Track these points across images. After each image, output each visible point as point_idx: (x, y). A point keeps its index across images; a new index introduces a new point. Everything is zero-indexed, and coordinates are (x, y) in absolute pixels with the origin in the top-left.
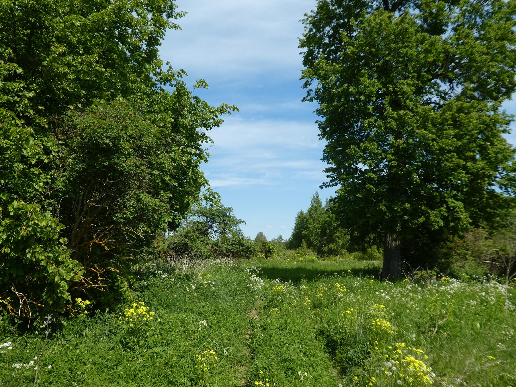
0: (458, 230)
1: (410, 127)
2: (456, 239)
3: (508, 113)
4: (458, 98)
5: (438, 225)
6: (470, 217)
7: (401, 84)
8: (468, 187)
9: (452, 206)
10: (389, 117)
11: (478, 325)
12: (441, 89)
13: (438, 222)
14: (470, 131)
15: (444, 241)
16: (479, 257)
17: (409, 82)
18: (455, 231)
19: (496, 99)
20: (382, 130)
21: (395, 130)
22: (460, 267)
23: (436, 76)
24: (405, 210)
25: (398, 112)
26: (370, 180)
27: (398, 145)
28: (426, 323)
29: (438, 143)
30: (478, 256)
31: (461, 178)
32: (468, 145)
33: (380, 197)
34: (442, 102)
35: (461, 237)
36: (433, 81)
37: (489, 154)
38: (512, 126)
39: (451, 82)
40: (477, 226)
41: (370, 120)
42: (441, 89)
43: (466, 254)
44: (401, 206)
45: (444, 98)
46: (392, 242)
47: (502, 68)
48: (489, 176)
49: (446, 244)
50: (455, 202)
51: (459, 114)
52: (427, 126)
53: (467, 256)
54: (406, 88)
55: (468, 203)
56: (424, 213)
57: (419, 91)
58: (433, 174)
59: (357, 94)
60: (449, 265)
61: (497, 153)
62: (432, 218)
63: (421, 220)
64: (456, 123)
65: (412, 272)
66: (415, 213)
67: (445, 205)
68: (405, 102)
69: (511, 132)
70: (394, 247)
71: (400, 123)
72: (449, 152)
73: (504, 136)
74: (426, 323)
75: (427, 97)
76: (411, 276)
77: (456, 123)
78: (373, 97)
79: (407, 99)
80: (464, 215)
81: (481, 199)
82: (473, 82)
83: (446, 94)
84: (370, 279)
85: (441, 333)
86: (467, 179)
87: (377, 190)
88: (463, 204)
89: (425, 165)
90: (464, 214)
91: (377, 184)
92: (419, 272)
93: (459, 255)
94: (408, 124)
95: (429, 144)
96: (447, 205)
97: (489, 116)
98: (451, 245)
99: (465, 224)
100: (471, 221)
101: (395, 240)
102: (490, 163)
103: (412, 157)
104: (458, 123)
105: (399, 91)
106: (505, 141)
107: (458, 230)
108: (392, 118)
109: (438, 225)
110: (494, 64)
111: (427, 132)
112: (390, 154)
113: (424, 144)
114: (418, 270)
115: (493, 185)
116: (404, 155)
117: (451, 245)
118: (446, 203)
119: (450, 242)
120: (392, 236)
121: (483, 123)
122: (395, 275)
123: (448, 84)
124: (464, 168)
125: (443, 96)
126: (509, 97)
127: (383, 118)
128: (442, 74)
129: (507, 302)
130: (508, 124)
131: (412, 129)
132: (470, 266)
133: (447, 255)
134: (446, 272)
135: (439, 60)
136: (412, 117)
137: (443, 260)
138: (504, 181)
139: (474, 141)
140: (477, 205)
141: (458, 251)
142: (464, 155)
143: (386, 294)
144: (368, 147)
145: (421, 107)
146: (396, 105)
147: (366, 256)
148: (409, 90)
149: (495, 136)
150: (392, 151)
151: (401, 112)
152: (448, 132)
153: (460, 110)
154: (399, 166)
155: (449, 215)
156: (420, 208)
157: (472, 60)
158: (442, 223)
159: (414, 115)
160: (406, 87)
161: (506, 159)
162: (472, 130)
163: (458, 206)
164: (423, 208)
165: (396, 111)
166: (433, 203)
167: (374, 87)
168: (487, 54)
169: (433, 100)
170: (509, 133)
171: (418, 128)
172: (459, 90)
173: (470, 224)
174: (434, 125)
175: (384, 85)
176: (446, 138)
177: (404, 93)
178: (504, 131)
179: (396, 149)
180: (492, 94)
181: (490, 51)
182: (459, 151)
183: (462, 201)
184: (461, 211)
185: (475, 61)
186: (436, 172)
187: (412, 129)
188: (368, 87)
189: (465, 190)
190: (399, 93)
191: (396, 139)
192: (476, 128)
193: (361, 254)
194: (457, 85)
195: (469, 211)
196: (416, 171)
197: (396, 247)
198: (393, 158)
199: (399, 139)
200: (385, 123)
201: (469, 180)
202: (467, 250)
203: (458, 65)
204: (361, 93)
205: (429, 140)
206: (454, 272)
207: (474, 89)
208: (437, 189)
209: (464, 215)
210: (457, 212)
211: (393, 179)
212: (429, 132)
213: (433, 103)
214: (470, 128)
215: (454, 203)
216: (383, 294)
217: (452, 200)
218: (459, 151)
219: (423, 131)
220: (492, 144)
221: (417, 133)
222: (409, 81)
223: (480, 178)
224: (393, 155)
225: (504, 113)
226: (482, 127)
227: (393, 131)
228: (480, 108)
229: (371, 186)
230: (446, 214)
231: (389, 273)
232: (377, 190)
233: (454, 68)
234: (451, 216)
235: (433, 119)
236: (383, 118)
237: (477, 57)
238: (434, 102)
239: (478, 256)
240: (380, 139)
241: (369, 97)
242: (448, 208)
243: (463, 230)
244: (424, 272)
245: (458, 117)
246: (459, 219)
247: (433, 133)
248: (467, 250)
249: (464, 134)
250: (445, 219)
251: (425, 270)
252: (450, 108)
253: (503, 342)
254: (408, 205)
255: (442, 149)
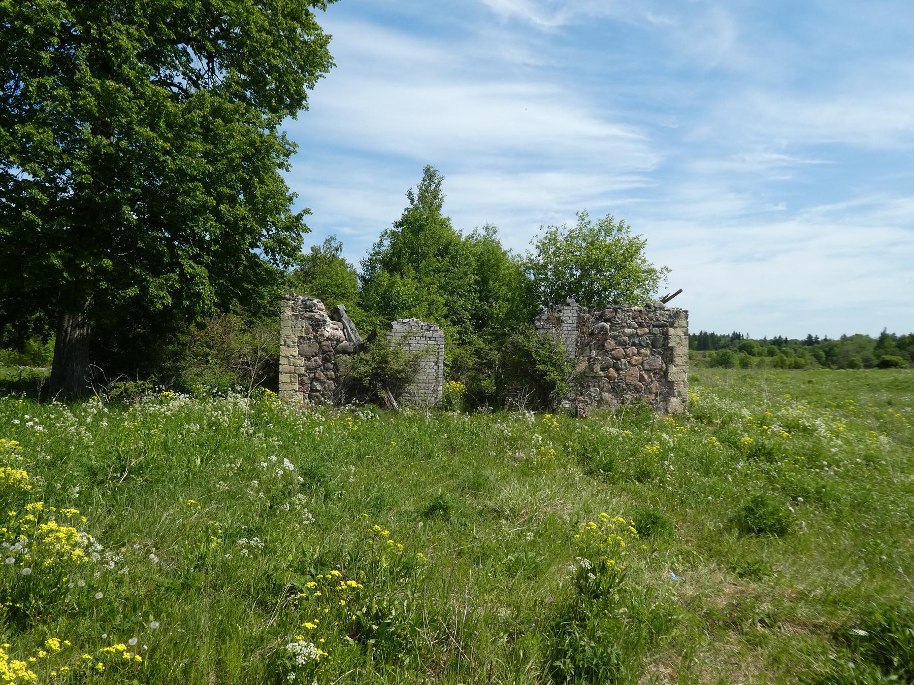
0: (195, 314)
1: (126, 116)
2: (193, 328)
3: (290, 138)
4: (214, 92)
5: (163, 304)
6: (217, 294)
7: (114, 29)
8: (219, 244)
9: (190, 274)
10: (83, 87)
11: (198, 461)
12: (192, 65)
13: (163, 298)
14: (230, 152)
15: (173, 331)
16: (227, 358)
17: (131, 31)
18: (190, 314)
19: (274, 110)
20: (66, 108)
21: (94, 115)
22: (196, 375)
23: (188, 41)
24: (101, 271)
25: (104, 82)
26: (32, 203)
27: (98, 146)
28: (109, 466)
29: (174, 160)
30: (226, 359)
31: (208, 230)
32: (224, 175)
33: (53, 242)
34: (193, 90)
35: (201, 326)
36: (180, 46)
37: (255, 196)
38: (292, 160)
39: (210, 59)
40: (227, 310)
41: (42, 80)
42: (192, 65)
43: (208, 355)
44: (94, 262)
45: (196, 85)
46: (74, 328)
47: (290, 65)
48: (251, 231)
49: (175, 336)
50: (196, 266)
51: (214, 118)
52: (157, 124)
53: (209, 358)
54: (124, 41)
55: (215, 272)
56: (139, 281)
57: (154, 57)
58: (163, 212)
59: (17, 19)
60: (177, 370)
61: (266, 197)
62: (153, 290)
63: (132, 291)
64: (208, 134)
65: (106, 385)
66: (121, 278)
67: (177, 270)
68: (120, 67)
69: (290, 169)
70: (77, 340)
71: (107, 104)
72: (194, 179)
73: (280, 172)
74: (109, 466)
75: (168, 72)
76: (104, 392)
77: (208, 134)
78: (54, 35)
79: (125, 62)
80: (207, 290)
81: (237, 267)
82: (241, 71)
83: (199, 76)
84: (18, 398)
85: (133, 479)
86: (218, 232)
87: (46, 226)
88: (206, 271)
89: (148, 193)
90: (207, 288)
91: (44, 213)
92: (121, 384)
93: (196, 355)
94: (122, 110)
95: (157, 158)
96: (182, 270)
97: (261, 136)
98: (183, 338)
99: (207, 305)
100: (216, 300)
101: (81, 326)
102: (254, 210)
103: (126, 178)
104: (212, 134)
105: (109, 42)
106: (282, 181)
107: (195, 314)
108: (91, 90)
109: (163, 304)
110: (276, 52)
111: (155, 135)
112: (79, 159)
113: (146, 152)
114: (119, 380)
115: (258, 247)
116: (106, 167)
117: (183, 338)
118: (180, 266)
119: (183, 333)
120: (74, 317)
121: (252, 144)
122: (75, 390)
123: (205, 61)
124: (215, 211)
125: (195, 79)
126: (293, 114)
127: (74, 86)
128: (195, 39)
129: (246, 423)
130: (287, 155)
131: (130, 123)
132: (213, 373)
133: (176, 356)
134: (168, 383)
135: (192, 12)
136: (131, 99)
137: (168, 364)
138: (271, 243)
139: (235, 170)
140: (230, 276)
141: (195, 349)
142: (215, 190)
143: (36, 423)
144: (33, 135)
145: (151, 85)
146: (103, 66)
147: (25, 358)
148: (130, 46)
149: (267, 169)
150: (84, 154)
151: (109, 83)
152: (194, 144)
153: (217, 112)
154: (95, 187)
155: (182, 288)
156: (132, 271)
157: (246, 33)
158: (169, 301)
159: (136, 98)
160: (126, 38)
161: (277, 209)
162: (234, 151)
163: (198, 274)
164: (138, 270)
165: (99, 79)
166: (156, 267)
167: (57, 16)
168: (268, 32)
169: (176, 80)
170: (287, 170)
171: (141, 123)
172: (221, 76)
173: (216, 305)
174: (169, 126)
175: (81, 20)
176: (189, 155)
177: (118, 49)
178: (280, 166)
179: (94, 152)
180: (270, 102)
181: (274, 29)
182: (211, 183)
183: (207, 266)
184: (202, 283)
185: (250, 37)
186: (166, 211)
187: (130, 123)
188: (44, 11)
189: (213, 248)
190: (110, 46)
191: (94, 132)
192: (239, 149)
193: (15, 354)
194: (221, 68)
195: (216, 284)
196: (132, 203)
197: (82, 339)
198: (85, 168)
199: (102, 133)
200: (75, 96)
201: (221, 234)
202: (210, 348)
203: (225, 35)
204: (27, 20)
205: (157, 151)
206: (184, 382)
207: (244, 85)
208: (169, 243)
209: (207, 290)
210: (197, 284)
211: (82, 208)
212: (159, 136)
213: (175, 86)
214: (229, 147)
215: (193, 268)
216: (30, 424)
217: (191, 262)
218: (211, 183)
219: (147, 131)
220: (262, 182)
221: (136, 133)
222: (133, 29)
223: (238, 233)
224: (85, 163)
225: (283, 137)
226: (250, 151)
227: (87, 116)
228: (250, 119)
229: (33, 217)
230: (177, 286)
231: (64, 387)
232: (46, 226)
233: (218, 36)
234: (185, 291)
235: (168, 115)
236: (74, 86)
237: (254, 30)
238: (179, 86)
239: (226, 359)
240: (64, 127)
241: (45, 31)
242: (182, 275)
243: (203, 314)
244: (131, 384)
245: (212, 123)
246: (198, 295)
247: (166, 140)
248: (210, 347)
249: (219, 155)
250: (176, 294)
251: (134, 380)
252: (201, 106)
253: (225, 479)
254: (108, 263)
255: (180, 172)
